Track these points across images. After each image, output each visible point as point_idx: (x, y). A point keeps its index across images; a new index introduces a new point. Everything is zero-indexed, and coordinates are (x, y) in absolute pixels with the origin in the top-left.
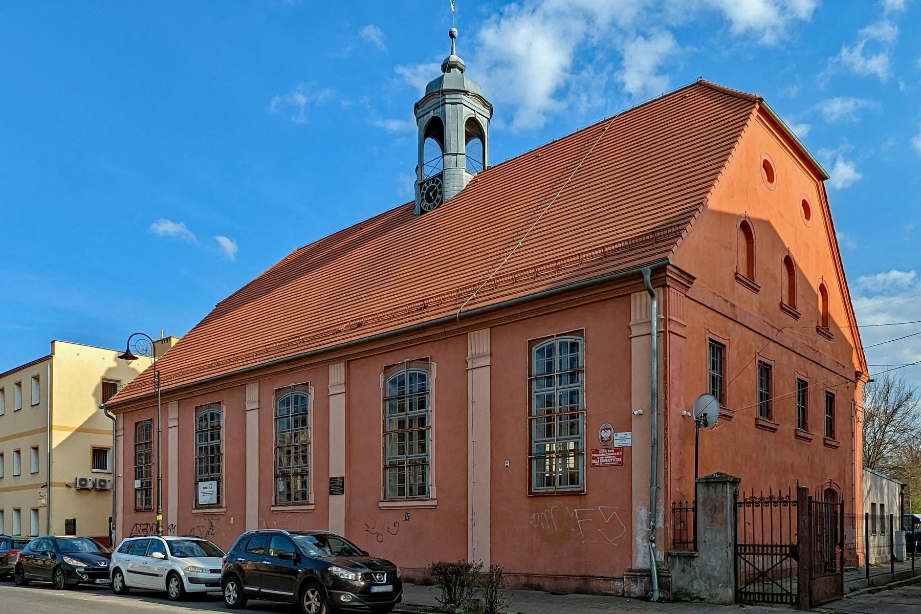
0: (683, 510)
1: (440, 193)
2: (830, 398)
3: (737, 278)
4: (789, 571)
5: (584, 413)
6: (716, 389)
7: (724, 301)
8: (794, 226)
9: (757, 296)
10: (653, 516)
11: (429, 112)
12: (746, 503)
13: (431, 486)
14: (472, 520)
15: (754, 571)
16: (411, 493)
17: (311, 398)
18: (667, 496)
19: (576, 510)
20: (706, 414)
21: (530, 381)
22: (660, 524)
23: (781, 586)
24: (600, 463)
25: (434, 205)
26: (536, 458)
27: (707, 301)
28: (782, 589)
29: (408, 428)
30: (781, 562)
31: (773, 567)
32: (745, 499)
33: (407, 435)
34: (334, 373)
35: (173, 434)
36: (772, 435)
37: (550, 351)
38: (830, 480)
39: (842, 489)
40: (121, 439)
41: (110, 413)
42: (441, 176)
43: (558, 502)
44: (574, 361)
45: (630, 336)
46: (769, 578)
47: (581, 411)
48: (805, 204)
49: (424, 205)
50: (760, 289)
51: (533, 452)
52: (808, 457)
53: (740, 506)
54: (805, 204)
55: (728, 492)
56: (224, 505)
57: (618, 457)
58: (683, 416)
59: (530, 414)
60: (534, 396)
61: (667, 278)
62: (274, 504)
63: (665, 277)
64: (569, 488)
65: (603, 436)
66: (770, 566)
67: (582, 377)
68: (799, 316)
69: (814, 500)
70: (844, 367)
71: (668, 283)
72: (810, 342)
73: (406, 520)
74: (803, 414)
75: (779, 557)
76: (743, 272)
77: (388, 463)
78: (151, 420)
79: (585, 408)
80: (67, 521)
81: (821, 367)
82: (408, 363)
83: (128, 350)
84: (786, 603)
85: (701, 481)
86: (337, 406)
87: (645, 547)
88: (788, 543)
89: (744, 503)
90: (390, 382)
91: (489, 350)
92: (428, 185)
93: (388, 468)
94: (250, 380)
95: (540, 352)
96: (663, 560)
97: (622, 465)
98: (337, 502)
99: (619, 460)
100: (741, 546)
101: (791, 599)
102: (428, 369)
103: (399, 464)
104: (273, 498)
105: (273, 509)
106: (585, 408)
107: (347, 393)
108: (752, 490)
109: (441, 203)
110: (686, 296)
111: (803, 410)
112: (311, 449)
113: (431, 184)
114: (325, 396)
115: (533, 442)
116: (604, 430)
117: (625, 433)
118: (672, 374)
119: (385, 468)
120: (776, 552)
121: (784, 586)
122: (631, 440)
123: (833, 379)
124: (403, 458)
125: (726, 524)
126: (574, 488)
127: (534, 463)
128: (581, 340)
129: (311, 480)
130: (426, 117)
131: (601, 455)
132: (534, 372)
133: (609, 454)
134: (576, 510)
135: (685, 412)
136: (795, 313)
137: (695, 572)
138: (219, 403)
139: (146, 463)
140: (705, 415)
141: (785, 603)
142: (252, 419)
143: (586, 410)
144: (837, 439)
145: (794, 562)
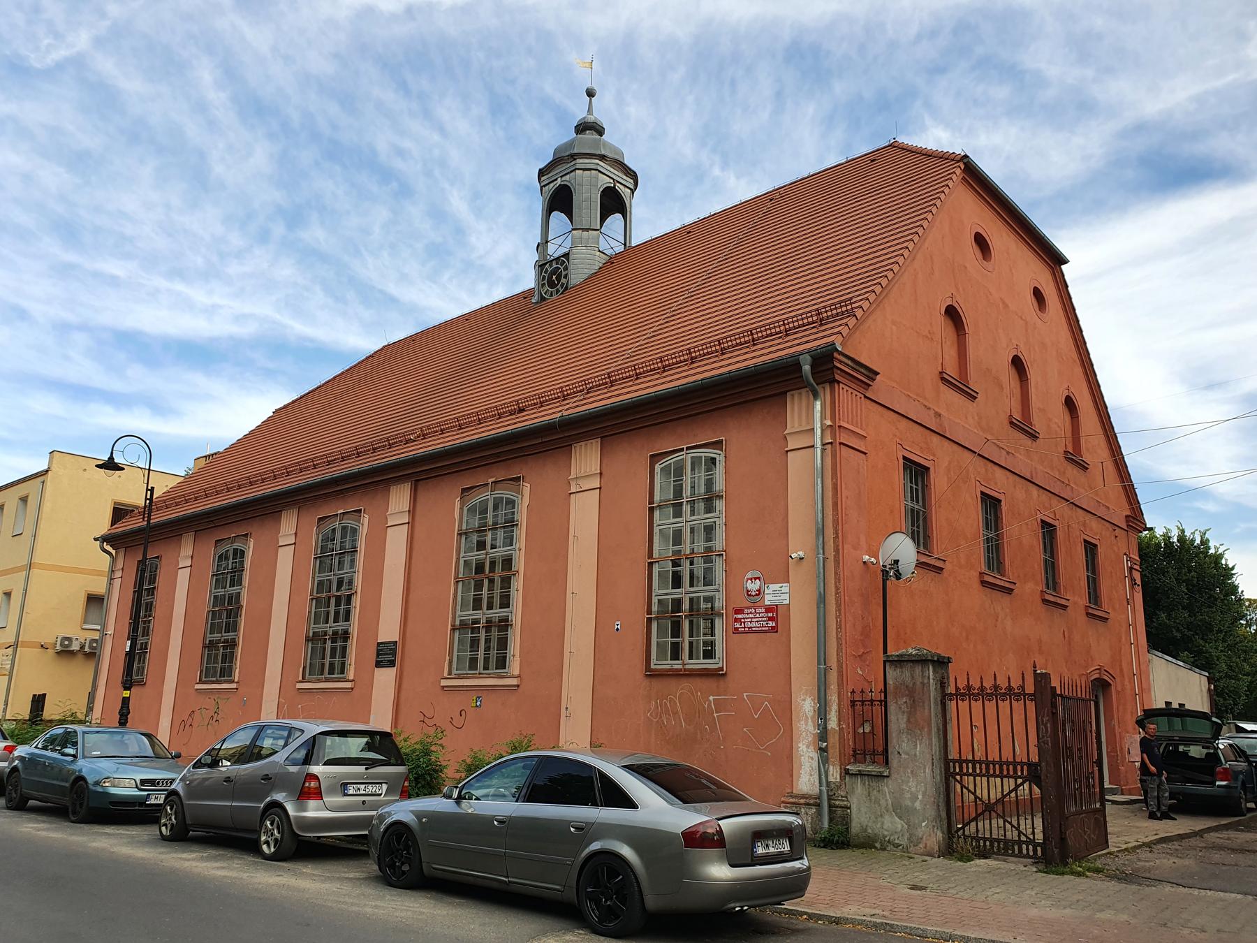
0: (867, 703)
1: (565, 276)
2: (1090, 548)
3: (942, 379)
4: (1028, 803)
5: (722, 554)
6: (992, 554)
7: (924, 408)
8: (1024, 318)
9: (975, 404)
10: (822, 713)
11: (556, 179)
12: (959, 695)
13: (514, 656)
14: (567, 708)
15: (976, 802)
16: (486, 668)
17: (364, 531)
18: (842, 680)
19: (711, 698)
20: (898, 561)
21: (651, 510)
22: (833, 724)
23: (1018, 829)
24: (745, 628)
25: (558, 291)
26: (657, 618)
27: (898, 406)
28: (1020, 833)
29: (487, 573)
30: (1016, 789)
31: (1004, 796)
32: (957, 688)
33: (486, 582)
34: (403, 503)
35: (183, 577)
36: (1005, 599)
37: (679, 470)
38: (1099, 665)
39: (1118, 680)
40: (117, 583)
41: (109, 548)
42: (566, 255)
43: (686, 685)
44: (710, 483)
45: (786, 449)
46: (998, 815)
47: (719, 551)
48: (1037, 294)
49: (545, 291)
50: (979, 396)
51: (653, 610)
52: (1064, 631)
53: (951, 700)
54: (1037, 294)
55: (931, 677)
56: (236, 680)
57: (771, 619)
58: (864, 562)
59: (650, 556)
60: (656, 530)
61: (835, 370)
62: (300, 678)
63: (832, 368)
64: (700, 663)
65: (749, 588)
66: (999, 795)
67: (719, 505)
68: (1037, 435)
69: (1058, 692)
70: (1108, 508)
71: (837, 377)
72: (1057, 473)
73: (477, 706)
74: (1051, 568)
75: (1012, 781)
76: (1017, 416)
77: (458, 623)
78: (157, 557)
79: (724, 549)
80: (34, 696)
81: (1074, 507)
82: (494, 484)
83: (111, 458)
84: (1028, 856)
85: (891, 659)
86: (396, 541)
87: (812, 759)
88: (1025, 760)
89: (956, 695)
90: (468, 509)
91: (599, 468)
92: (551, 266)
93: (457, 629)
94: (289, 505)
95: (666, 470)
96: (838, 780)
97: (777, 632)
98: (385, 677)
99: (772, 624)
100: (954, 761)
101: (1035, 851)
102: (519, 492)
103: (472, 624)
104: (301, 669)
105: (299, 686)
106: (724, 549)
107: (411, 524)
108: (981, 678)
109: (567, 288)
110: (865, 397)
111: (1094, 580)
112: (357, 601)
113: (555, 266)
114: (380, 530)
115: (654, 594)
116: (751, 579)
117: (781, 585)
118: (846, 502)
119: (454, 629)
120: (981, 772)
121: (1022, 828)
122: (788, 595)
123: (1094, 524)
124: (477, 614)
125: (930, 725)
126: (709, 664)
127: (654, 626)
128: (720, 455)
129: (353, 645)
130: (552, 185)
131: (747, 616)
132: (657, 498)
133: (758, 616)
134: (711, 698)
135: (867, 557)
136: (1031, 431)
137: (887, 800)
138: (246, 535)
139: (145, 616)
140: (896, 562)
141: (1024, 857)
142: (285, 558)
143: (725, 551)
144: (1105, 606)
145: (1036, 790)
